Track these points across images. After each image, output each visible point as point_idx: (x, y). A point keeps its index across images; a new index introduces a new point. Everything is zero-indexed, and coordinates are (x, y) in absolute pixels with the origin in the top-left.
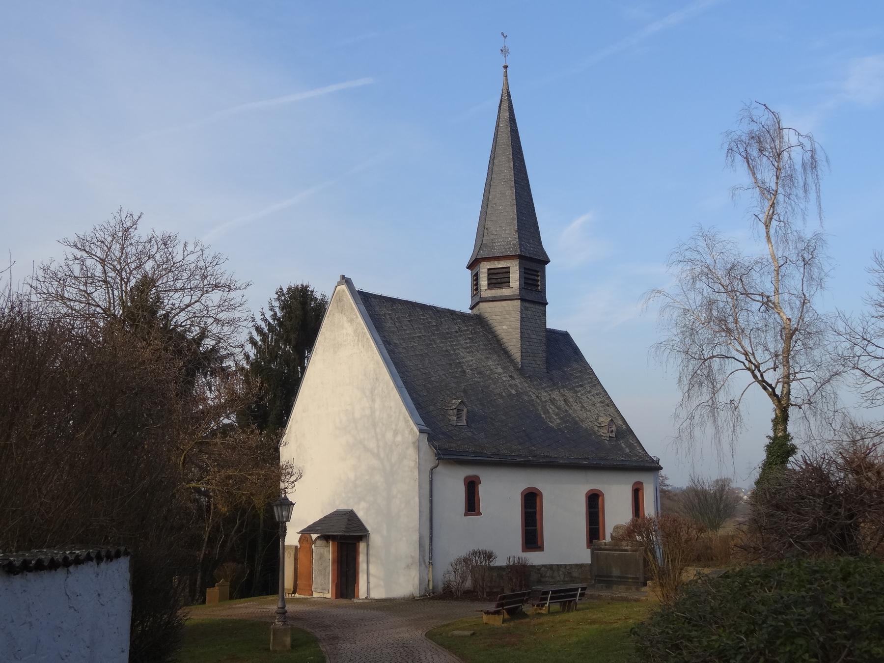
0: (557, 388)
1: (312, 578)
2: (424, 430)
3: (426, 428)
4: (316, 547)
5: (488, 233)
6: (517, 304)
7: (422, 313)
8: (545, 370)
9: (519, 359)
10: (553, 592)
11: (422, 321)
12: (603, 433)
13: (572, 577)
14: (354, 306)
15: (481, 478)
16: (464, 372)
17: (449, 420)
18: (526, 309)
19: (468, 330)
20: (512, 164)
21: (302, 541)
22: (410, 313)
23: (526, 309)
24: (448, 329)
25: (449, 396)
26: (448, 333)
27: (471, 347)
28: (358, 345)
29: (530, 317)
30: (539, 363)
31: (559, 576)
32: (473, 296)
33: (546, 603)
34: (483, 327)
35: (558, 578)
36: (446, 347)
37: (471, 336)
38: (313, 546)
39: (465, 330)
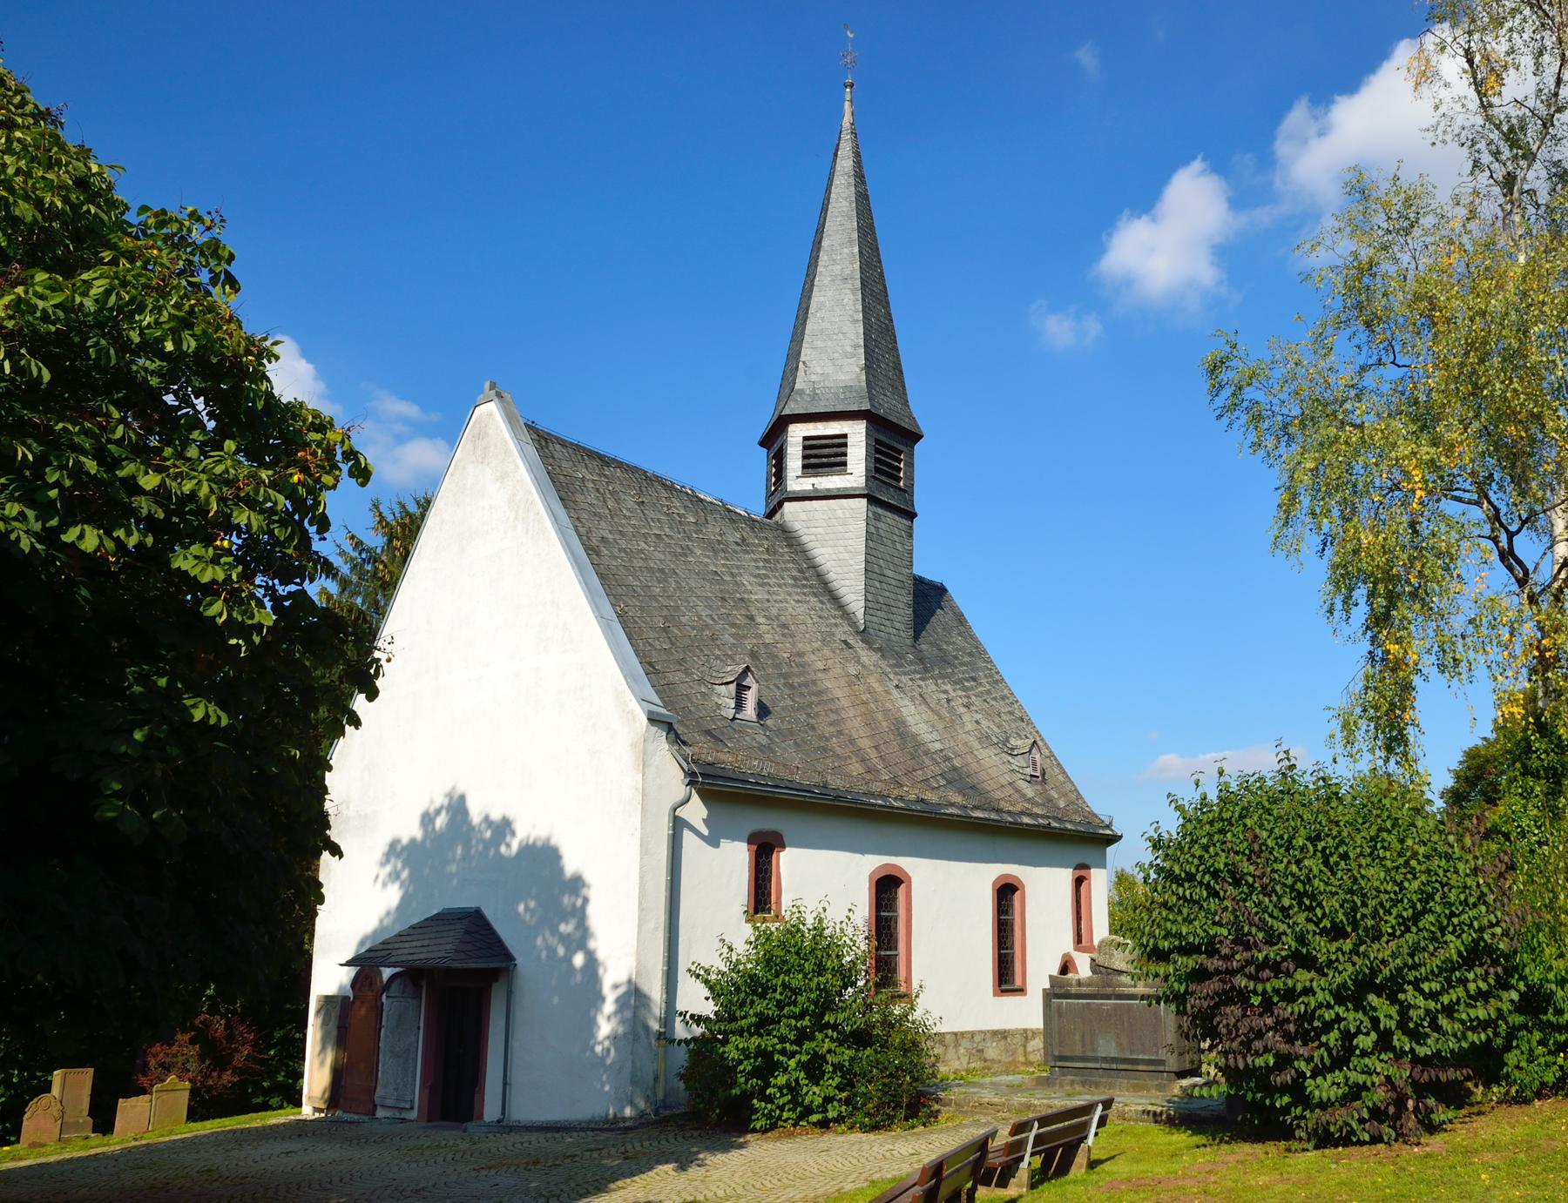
0: (933, 677)
1: (377, 1070)
2: (658, 714)
3: (664, 711)
4: (391, 1000)
5: (805, 372)
6: (859, 506)
7: (666, 495)
8: (909, 642)
9: (860, 614)
10: (1043, 1121)
11: (665, 509)
13: (986, 1061)
14: (512, 445)
15: (785, 838)
16: (752, 618)
17: (718, 706)
18: (877, 517)
19: (762, 545)
20: (856, 250)
21: (358, 985)
23: (877, 517)
25: (717, 657)
27: (767, 576)
30: (898, 625)
31: (959, 1059)
32: (770, 495)
33: (1021, 1159)
34: (790, 546)
35: (957, 1063)
36: (715, 565)
37: (766, 557)
38: (384, 997)
39: (754, 544)
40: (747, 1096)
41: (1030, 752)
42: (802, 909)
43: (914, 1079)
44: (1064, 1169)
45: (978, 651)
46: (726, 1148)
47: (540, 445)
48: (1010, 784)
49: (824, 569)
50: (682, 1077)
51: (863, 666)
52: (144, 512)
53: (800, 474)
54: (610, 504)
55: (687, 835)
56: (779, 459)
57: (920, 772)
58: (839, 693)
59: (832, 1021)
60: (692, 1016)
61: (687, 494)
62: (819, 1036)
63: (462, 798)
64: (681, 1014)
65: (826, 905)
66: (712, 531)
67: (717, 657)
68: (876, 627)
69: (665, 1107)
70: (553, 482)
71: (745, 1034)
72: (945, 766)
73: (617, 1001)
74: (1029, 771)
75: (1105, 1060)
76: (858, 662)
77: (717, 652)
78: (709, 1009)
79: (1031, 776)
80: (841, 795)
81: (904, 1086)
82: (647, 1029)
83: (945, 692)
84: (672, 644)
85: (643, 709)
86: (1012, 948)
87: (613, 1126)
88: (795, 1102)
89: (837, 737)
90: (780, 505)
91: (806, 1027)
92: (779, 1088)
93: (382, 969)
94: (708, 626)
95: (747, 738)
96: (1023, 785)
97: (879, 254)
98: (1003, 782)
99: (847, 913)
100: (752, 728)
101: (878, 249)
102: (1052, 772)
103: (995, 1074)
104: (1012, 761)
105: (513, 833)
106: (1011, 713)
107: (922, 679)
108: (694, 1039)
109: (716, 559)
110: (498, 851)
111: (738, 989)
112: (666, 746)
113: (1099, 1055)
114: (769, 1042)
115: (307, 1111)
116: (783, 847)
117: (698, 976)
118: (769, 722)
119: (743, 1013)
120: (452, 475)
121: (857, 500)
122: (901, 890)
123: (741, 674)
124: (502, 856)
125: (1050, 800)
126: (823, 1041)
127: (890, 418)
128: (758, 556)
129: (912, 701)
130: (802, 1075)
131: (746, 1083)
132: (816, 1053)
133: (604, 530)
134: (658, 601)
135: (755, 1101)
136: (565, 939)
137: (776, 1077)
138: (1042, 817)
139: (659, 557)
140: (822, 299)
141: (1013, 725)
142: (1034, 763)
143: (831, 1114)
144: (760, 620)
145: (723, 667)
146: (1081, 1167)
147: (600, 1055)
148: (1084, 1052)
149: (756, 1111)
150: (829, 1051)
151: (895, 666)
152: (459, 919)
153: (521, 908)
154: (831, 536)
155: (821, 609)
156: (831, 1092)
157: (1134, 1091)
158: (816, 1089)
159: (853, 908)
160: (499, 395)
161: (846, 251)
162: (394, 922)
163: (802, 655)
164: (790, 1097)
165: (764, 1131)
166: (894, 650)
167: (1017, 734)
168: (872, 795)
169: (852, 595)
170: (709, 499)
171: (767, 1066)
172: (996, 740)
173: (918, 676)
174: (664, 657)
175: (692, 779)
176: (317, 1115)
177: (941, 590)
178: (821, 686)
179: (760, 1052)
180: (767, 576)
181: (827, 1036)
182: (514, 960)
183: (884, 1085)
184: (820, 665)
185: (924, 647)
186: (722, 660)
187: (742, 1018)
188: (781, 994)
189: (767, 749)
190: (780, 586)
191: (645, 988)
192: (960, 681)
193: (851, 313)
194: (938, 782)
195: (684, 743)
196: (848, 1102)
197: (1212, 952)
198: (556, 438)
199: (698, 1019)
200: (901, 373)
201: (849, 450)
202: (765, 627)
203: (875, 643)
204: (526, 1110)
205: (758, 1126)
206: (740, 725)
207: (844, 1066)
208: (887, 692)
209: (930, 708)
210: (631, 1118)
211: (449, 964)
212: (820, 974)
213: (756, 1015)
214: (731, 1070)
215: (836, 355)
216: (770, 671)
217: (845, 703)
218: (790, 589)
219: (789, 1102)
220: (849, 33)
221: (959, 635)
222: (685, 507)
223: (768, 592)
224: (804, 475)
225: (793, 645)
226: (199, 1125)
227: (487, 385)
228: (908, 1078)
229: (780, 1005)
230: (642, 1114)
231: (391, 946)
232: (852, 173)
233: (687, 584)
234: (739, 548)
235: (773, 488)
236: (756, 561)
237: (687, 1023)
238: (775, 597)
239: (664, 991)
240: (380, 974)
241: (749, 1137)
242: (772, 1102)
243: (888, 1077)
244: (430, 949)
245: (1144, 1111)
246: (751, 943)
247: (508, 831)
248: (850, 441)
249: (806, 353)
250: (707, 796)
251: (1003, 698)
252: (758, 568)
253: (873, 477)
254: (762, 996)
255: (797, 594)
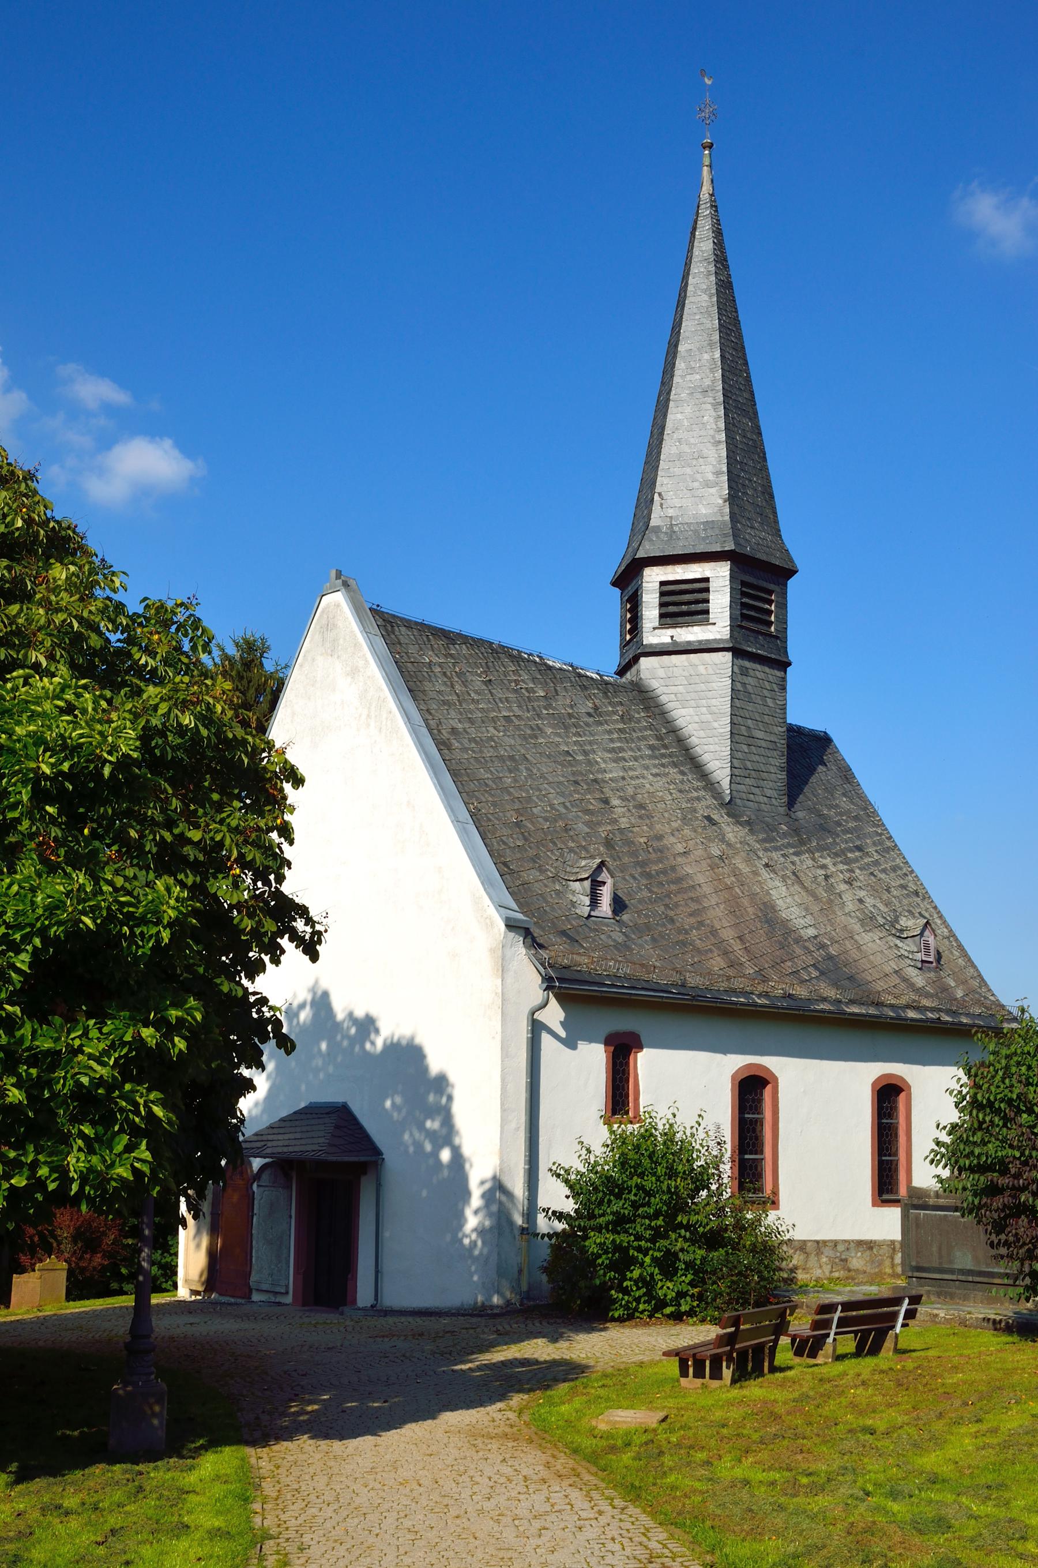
0: (810, 851)
2: (515, 920)
3: (520, 916)
4: (262, 1189)
5: (661, 505)
6: (724, 660)
7: (514, 668)
8: (782, 810)
9: (725, 783)
10: (847, 1306)
11: (513, 684)
12: (909, 952)
13: (849, 1270)
14: (360, 638)
15: (642, 1039)
16: (606, 801)
17: (573, 904)
18: (744, 672)
19: (615, 713)
20: (717, 354)
22: (488, 667)
23: (744, 672)
24: (572, 707)
25: (571, 850)
26: (570, 716)
27: (621, 749)
28: (368, 725)
29: (751, 691)
30: (769, 793)
31: (821, 1267)
32: (625, 645)
33: (828, 1335)
34: (647, 709)
35: (819, 1271)
36: (567, 744)
37: (621, 726)
39: (608, 714)
40: (605, 1288)
41: (921, 934)
42: (653, 1114)
43: (762, 1278)
44: (875, 1350)
45: (867, 813)
46: (591, 1330)
47: (387, 631)
48: (896, 972)
49: (685, 732)
50: (545, 1270)
51: (729, 845)
52: (192, 858)
53: (657, 624)
54: (458, 688)
55: (546, 1038)
56: (633, 604)
57: (789, 964)
58: (701, 879)
59: (685, 1222)
60: (554, 1213)
61: (535, 662)
62: (673, 1236)
63: (326, 995)
64: (544, 1210)
65: (676, 1111)
66: (562, 704)
67: (571, 850)
68: (744, 796)
69: (529, 1298)
70: (401, 672)
71: (604, 1231)
72: (819, 955)
73: (483, 1196)
74: (919, 956)
75: (962, 1272)
76: (723, 840)
77: (571, 844)
78: (569, 1206)
79: (923, 961)
80: (700, 993)
81: (753, 1285)
82: (511, 1223)
83: (824, 867)
84: (526, 839)
85: (501, 916)
86: (896, 1154)
87: (482, 1312)
88: (650, 1295)
89: (697, 929)
90: (635, 659)
91: (661, 1226)
92: (635, 1281)
93: (252, 1159)
94: (560, 816)
95: (602, 937)
96: (912, 973)
97: (745, 354)
98: (888, 969)
99: (697, 1118)
100: (607, 925)
101: (743, 347)
102: (951, 956)
103: (858, 1284)
104: (900, 944)
105: (377, 1031)
106: (903, 887)
107: (796, 854)
108: (556, 1234)
109: (568, 737)
110: (363, 1047)
111: (596, 1189)
112: (523, 951)
113: (956, 1266)
114: (623, 1239)
115: (183, 1293)
116: (640, 1047)
117: (558, 1176)
118: (625, 917)
119: (601, 1212)
120: (301, 666)
121: (720, 653)
122: (767, 1092)
123: (596, 869)
124: (367, 1054)
125: (945, 989)
126: (676, 1240)
127: (759, 556)
128: (613, 726)
129: (784, 881)
130: (657, 1271)
131: (605, 1275)
132: (668, 1251)
133: (453, 720)
134: (510, 794)
135: (613, 1292)
136: (432, 1135)
137: (632, 1272)
138: (932, 1010)
139: (509, 742)
140: (679, 416)
141: (905, 902)
142: (927, 947)
143: (684, 1308)
144: (615, 802)
145: (577, 861)
146: (889, 1350)
147: (467, 1247)
148: (940, 1263)
149: (614, 1301)
150: (682, 1250)
151: (764, 840)
152: (327, 1113)
153: (388, 1104)
154: (693, 695)
155: (682, 782)
156: (685, 1288)
157: (989, 1304)
158: (670, 1284)
159: (703, 1113)
160: (346, 584)
161: (706, 356)
162: (263, 1111)
163: (659, 838)
164: (645, 1290)
165: (621, 1320)
166: (764, 822)
167: (909, 911)
168: (734, 992)
169: (717, 763)
170: (558, 665)
171: (623, 1261)
172: (881, 921)
173: (792, 851)
174: (518, 855)
175: (549, 984)
176: (193, 1298)
177: (823, 741)
178: (681, 872)
179: (618, 1248)
180: (621, 749)
181: (680, 1236)
182: (382, 1154)
183: (733, 1282)
184: (680, 848)
185: (800, 814)
186: (575, 853)
187: (600, 1216)
188: (636, 1195)
189: (623, 947)
190: (636, 759)
191: (508, 1184)
192: (843, 852)
193: (712, 432)
194: (809, 974)
195: (541, 946)
196: (700, 1297)
197: (1004, 1171)
198: (402, 619)
199: (560, 1216)
200: (772, 496)
201: (712, 597)
202: (620, 810)
203: (742, 816)
204: (396, 1296)
205: (616, 1315)
206: (595, 923)
207: (696, 1264)
208: (756, 873)
209: (804, 888)
210: (498, 1307)
211: (324, 1157)
212: (670, 1178)
213: (613, 1213)
214: (591, 1262)
215: (696, 484)
216: (626, 860)
217: (707, 889)
218: (647, 762)
219: (644, 1294)
220: (706, 80)
221: (844, 795)
222: (534, 680)
223: (624, 769)
224: (663, 626)
225: (651, 827)
226: (78, 1303)
227: (333, 573)
228: (756, 1278)
229: (635, 1205)
230: (508, 1303)
231: (264, 1138)
232: (712, 258)
233: (539, 770)
234: (591, 719)
235: (628, 637)
236: (610, 732)
237: (550, 1219)
238: (631, 773)
239: (526, 1188)
240: (250, 1164)
241: (608, 1325)
242: (629, 1295)
243: (737, 1275)
244: (303, 1142)
245: (984, 1319)
246: (608, 1146)
247: (372, 1029)
248: (712, 585)
249: (663, 483)
250: (564, 999)
251: (894, 869)
252: (612, 740)
253: (740, 626)
254: (618, 1197)
255: (655, 766)
